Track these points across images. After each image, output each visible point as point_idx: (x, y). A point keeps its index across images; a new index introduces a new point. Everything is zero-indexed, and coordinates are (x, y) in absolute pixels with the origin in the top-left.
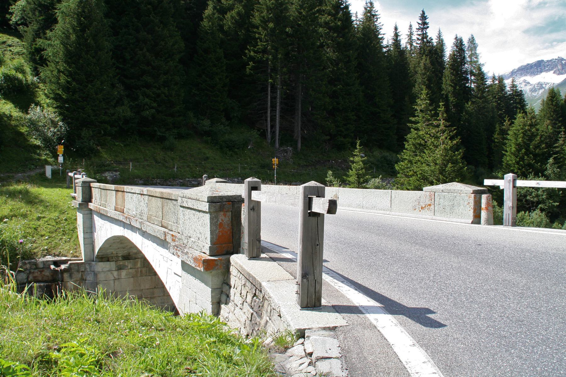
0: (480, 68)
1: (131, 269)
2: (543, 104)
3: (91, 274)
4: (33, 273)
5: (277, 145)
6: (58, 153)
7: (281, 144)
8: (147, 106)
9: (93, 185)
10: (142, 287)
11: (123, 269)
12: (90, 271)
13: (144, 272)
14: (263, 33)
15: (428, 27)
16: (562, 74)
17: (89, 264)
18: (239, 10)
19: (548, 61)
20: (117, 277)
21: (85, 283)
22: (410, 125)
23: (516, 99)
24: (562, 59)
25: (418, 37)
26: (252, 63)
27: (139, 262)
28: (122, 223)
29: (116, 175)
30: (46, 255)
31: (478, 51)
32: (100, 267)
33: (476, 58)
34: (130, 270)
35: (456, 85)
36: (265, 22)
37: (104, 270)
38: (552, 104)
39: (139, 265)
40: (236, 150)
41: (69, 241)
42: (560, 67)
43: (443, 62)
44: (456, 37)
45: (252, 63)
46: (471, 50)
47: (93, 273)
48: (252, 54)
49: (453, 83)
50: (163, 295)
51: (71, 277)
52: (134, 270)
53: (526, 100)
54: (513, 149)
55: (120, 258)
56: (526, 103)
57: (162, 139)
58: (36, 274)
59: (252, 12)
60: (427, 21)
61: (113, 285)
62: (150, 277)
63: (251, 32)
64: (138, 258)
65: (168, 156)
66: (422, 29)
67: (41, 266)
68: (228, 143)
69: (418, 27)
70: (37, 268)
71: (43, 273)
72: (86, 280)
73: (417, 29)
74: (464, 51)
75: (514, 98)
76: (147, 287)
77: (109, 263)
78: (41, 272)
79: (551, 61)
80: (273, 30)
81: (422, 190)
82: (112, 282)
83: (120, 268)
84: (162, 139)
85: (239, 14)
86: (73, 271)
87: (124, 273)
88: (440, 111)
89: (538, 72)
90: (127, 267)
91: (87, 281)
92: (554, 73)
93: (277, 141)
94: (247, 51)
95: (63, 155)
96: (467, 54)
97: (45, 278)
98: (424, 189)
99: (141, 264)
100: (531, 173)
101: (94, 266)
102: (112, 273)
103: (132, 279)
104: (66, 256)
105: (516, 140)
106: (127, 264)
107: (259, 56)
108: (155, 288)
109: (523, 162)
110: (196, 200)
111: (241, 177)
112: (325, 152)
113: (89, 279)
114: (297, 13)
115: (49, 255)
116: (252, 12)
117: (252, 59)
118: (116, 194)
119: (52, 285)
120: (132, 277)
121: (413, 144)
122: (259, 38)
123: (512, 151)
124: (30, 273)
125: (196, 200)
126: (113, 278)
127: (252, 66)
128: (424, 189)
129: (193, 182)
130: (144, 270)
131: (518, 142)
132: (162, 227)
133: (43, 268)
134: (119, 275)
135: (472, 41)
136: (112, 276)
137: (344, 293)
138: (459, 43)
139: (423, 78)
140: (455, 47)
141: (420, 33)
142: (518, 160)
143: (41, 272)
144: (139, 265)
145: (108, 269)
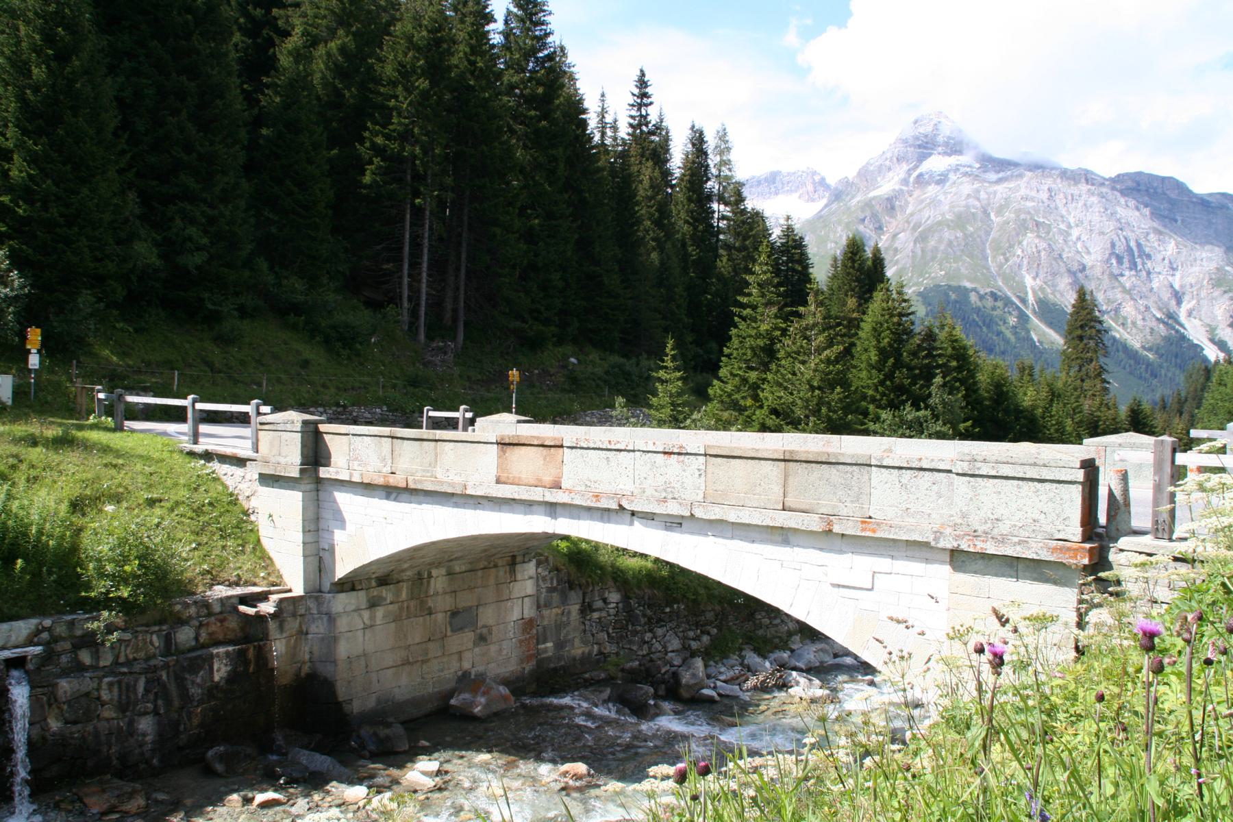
0: (739, 190)
1: (391, 603)
2: (835, 266)
3: (320, 618)
4: (208, 624)
5: (422, 337)
6: (29, 347)
7: (430, 338)
8: (189, 244)
9: (323, 428)
10: (410, 641)
11: (379, 605)
12: (320, 613)
13: (412, 609)
14: (406, 99)
15: (651, 103)
16: (813, 200)
17: (317, 598)
18: (344, 43)
19: (789, 174)
21: (306, 639)
22: (738, 310)
23: (793, 254)
24: (815, 173)
25: (632, 121)
26: (379, 159)
27: (405, 589)
28: (542, 509)
30: (213, 585)
31: (733, 156)
32: (342, 602)
34: (391, 607)
35: (696, 220)
36: (405, 73)
37: (347, 610)
38: (853, 267)
40: (358, 346)
41: (243, 552)
42: (810, 188)
43: (667, 173)
44: (693, 127)
45: (379, 159)
46: (721, 153)
47: (325, 618)
48: (379, 140)
49: (692, 218)
50: (440, 654)
51: (281, 628)
53: (810, 256)
54: (874, 358)
55: (374, 583)
56: (811, 262)
57: (213, 319)
58: (213, 628)
59: (378, 51)
60: (649, 90)
61: (361, 639)
62: (421, 618)
63: (372, 92)
64: (403, 581)
65: (233, 356)
66: (640, 106)
67: (217, 608)
68: (341, 330)
69: (632, 102)
70: (210, 614)
71: (226, 624)
72: (307, 633)
73: (629, 105)
74: (706, 154)
75: (789, 251)
76: (417, 640)
77: (354, 593)
78: (222, 621)
79: (794, 173)
80: (425, 95)
82: (360, 633)
83: (373, 604)
84: (213, 319)
85: (343, 50)
86: (285, 615)
87: (380, 612)
88: (811, 289)
89: (770, 193)
90: (385, 599)
91: (310, 636)
92: (800, 197)
93: (422, 329)
94: (367, 134)
95: (39, 352)
96: (713, 160)
97: (230, 636)
99: (407, 593)
100: (906, 401)
101: (330, 601)
102: (360, 616)
103: (393, 625)
104: (255, 584)
105: (879, 342)
106: (384, 595)
107: (395, 146)
108: (429, 640)
109: (891, 381)
111: (386, 405)
112: (507, 353)
113: (316, 630)
114: (466, 63)
115: (218, 584)
116: (378, 51)
117: (378, 151)
119: (247, 649)
120: (394, 621)
121: (752, 348)
122: (395, 108)
123: (873, 362)
124: (201, 625)
126: (362, 626)
127: (380, 167)
128: (1085, 441)
130: (412, 603)
131: (882, 345)
132: (784, 510)
133: (221, 613)
134: (373, 618)
135: (723, 136)
136: (360, 622)
137: (26, 707)
138: (698, 141)
139: (648, 207)
140: (690, 146)
141: (634, 113)
142: (881, 377)
143: (222, 621)
144: (404, 595)
145: (353, 607)
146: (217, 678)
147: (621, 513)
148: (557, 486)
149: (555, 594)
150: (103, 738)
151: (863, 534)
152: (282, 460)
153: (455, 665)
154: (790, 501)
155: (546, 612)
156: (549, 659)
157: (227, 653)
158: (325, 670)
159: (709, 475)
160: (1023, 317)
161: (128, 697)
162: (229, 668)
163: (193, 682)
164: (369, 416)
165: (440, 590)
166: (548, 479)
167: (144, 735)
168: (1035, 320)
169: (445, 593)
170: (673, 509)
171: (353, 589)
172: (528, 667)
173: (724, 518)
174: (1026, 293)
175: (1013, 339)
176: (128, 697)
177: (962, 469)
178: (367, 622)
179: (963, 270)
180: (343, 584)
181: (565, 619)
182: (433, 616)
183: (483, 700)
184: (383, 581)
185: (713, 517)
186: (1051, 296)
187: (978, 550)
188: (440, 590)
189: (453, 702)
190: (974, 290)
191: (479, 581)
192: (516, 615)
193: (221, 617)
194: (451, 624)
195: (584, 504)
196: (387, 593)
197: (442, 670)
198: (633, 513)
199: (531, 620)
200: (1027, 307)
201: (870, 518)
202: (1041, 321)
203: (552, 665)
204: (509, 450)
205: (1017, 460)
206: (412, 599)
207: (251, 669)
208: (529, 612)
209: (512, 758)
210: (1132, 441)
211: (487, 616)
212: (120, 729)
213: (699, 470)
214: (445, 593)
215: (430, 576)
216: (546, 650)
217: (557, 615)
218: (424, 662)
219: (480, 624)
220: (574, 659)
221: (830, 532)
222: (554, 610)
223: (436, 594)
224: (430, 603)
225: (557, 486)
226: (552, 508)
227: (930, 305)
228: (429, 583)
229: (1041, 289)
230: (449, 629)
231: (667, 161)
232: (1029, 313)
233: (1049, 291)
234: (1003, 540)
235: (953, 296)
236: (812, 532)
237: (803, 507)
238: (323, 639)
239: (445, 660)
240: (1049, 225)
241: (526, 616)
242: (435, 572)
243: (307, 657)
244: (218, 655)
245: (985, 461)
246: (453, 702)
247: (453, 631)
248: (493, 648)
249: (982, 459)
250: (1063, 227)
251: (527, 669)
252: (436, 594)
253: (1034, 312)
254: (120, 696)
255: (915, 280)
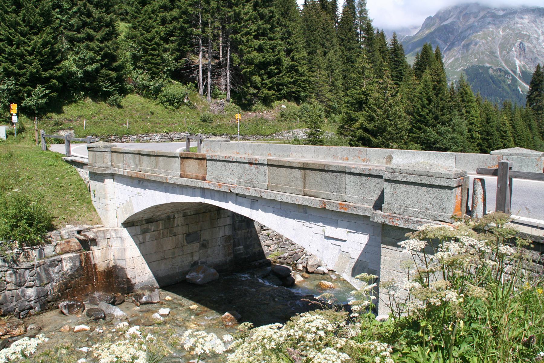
10: (165, 249)
20: (142, 241)
27: (161, 225)
29: (71, 133)
31: (367, 8)
33: (365, 14)
39: (161, 227)
47: (120, 239)
52: (157, 232)
55: (144, 222)
76: (169, 248)
77: (134, 227)
81: (489, 153)
83: (144, 232)
87: (148, 236)
90: (151, 230)
91: (113, 248)
95: (17, 115)
98: (492, 152)
102: (138, 238)
110: (256, 164)
113: (116, 245)
118: (182, 164)
125: (256, 164)
129: (145, 138)
130: (165, 231)
134: (144, 239)
144: (161, 227)
146: (65, 269)
147: (226, 195)
148: (204, 179)
149: (243, 223)
150: (9, 299)
151: (340, 211)
152: (97, 165)
153: (189, 259)
154: (307, 190)
155: (239, 232)
156: (242, 253)
157: (70, 258)
158: (121, 263)
159: (270, 175)
160: (514, 80)
161: (20, 280)
162: (71, 264)
163: (53, 272)
164: (179, 136)
165: (180, 224)
166: (200, 175)
167: (30, 297)
168: (520, 81)
169: (182, 225)
170: (252, 193)
171: (133, 225)
172: (229, 259)
173: (275, 199)
174: (516, 68)
175: (508, 90)
176: (20, 280)
177: (388, 177)
178: (142, 241)
179: (486, 58)
180: (127, 223)
181: (249, 235)
182: (177, 236)
183: (202, 276)
184: (149, 221)
185: (270, 198)
186: (528, 70)
187: (394, 224)
188: (180, 224)
189: (187, 276)
190: (490, 67)
191: (201, 219)
192: (221, 234)
193: (67, 240)
194: (186, 240)
195: (215, 189)
196: (152, 227)
197: (183, 261)
198: (237, 194)
199: (229, 236)
200: (516, 75)
201: (346, 201)
202: (523, 81)
203: (243, 257)
204: (185, 160)
205: (417, 172)
206: (165, 229)
207: (83, 264)
208: (228, 232)
209: (206, 309)
210: (518, 152)
211: (206, 235)
212: (18, 295)
213: (265, 172)
214: (182, 225)
215: (174, 218)
216: (239, 250)
217: (245, 233)
218: (173, 258)
219: (202, 239)
220: (255, 253)
221: (325, 208)
222: (243, 231)
223: (178, 226)
224: (175, 230)
225: (204, 179)
226: (204, 192)
227: (469, 75)
228: (174, 221)
229: (524, 66)
230: (185, 242)
231: (336, 11)
232: (517, 78)
233: (527, 67)
234: (408, 221)
235: (480, 71)
236: (316, 208)
237: (313, 194)
238: (119, 249)
239: (184, 256)
240: (529, 35)
241: (227, 234)
242: (176, 216)
243: (112, 258)
244: (65, 259)
245: (400, 172)
246: (187, 276)
247: (187, 243)
248: (210, 251)
249: (398, 171)
250: (536, 36)
251: (228, 259)
252: (178, 226)
253: (520, 77)
254: (16, 279)
255: (462, 64)
